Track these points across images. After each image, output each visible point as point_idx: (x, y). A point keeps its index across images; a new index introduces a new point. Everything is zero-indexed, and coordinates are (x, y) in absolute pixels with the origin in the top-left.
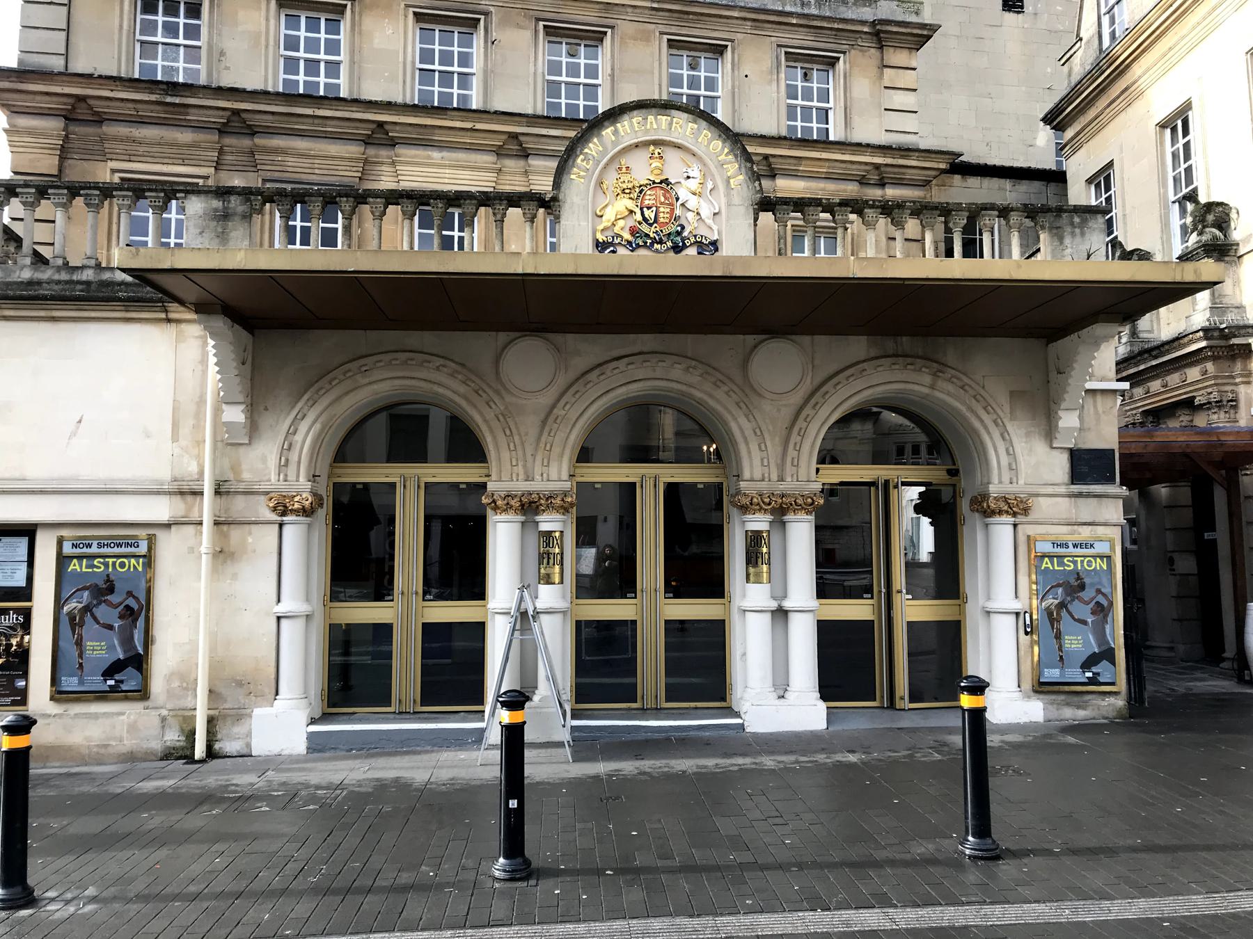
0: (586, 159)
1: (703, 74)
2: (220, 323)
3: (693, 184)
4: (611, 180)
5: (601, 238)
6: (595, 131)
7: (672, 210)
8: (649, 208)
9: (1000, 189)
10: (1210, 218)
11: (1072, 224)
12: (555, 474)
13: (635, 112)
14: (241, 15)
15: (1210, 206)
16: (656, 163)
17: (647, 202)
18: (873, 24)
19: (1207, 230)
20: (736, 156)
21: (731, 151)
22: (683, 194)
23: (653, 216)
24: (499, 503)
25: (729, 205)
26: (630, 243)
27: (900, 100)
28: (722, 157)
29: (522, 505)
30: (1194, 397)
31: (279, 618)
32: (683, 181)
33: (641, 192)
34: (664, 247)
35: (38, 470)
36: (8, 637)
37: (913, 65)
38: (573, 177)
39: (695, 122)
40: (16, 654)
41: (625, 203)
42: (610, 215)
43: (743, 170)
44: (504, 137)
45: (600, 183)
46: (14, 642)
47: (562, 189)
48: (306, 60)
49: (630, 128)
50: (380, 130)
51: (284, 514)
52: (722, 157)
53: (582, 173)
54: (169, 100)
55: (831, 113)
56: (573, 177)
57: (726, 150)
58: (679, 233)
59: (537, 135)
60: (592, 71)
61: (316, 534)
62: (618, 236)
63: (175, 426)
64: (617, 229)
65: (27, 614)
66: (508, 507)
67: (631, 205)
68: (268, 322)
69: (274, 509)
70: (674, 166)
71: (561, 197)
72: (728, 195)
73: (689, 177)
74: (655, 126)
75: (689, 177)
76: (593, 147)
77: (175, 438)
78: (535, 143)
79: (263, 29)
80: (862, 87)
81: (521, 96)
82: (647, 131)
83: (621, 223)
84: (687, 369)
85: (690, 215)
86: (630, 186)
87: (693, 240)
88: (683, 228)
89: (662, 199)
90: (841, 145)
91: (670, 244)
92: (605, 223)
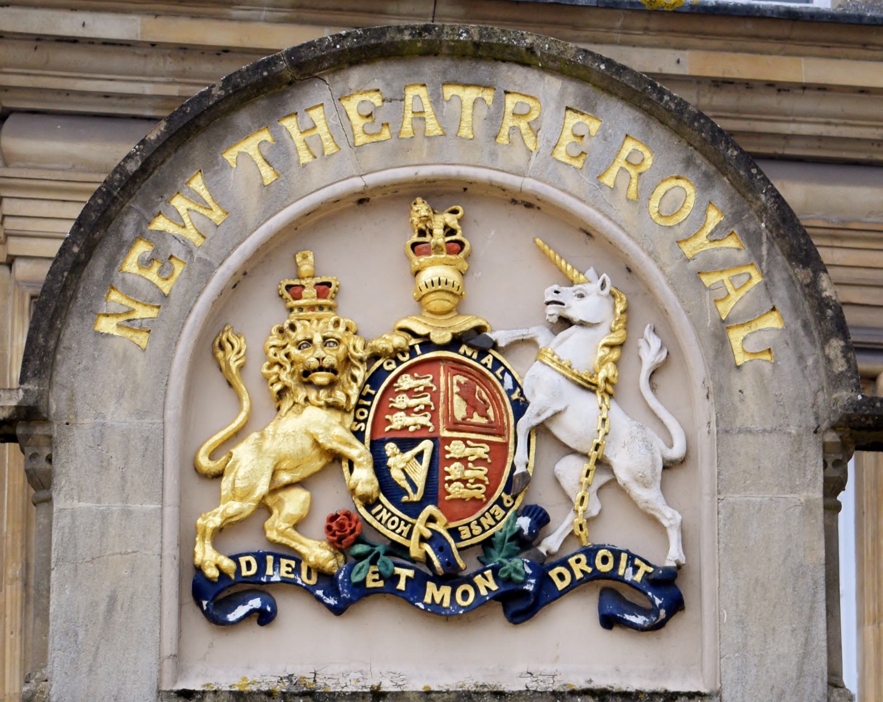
0: (160, 258)
3: (580, 350)
4: (256, 337)
5: (210, 558)
6: (197, 149)
7: (499, 452)
8: (406, 443)
13: (355, 76)
16: (436, 270)
17: (398, 420)
20: (751, 240)
22: (542, 385)
23: (420, 474)
25: (725, 429)
26: (326, 578)
28: (700, 244)
32: (542, 336)
33: (374, 380)
38: (106, 325)
39: (586, 108)
41: (311, 424)
42: (247, 469)
43: (781, 293)
44: (251, 226)
45: (211, 345)
47: (62, 373)
52: (700, 244)
53: (142, 313)
56: (106, 325)
57: (714, 217)
58: (523, 543)
59: (39, 39)
62: (282, 552)
64: (277, 528)
67: (334, 430)
70: (506, 283)
71: (56, 404)
72: (719, 391)
73: (565, 322)
74: (433, 127)
75: (565, 322)
76: (188, 211)
78: (26, 69)
82: (400, 149)
83: (295, 502)
84: (406, 428)
85: (571, 471)
86: (331, 357)
87: (580, 568)
88: (541, 519)
89: (460, 409)
91: (487, 584)
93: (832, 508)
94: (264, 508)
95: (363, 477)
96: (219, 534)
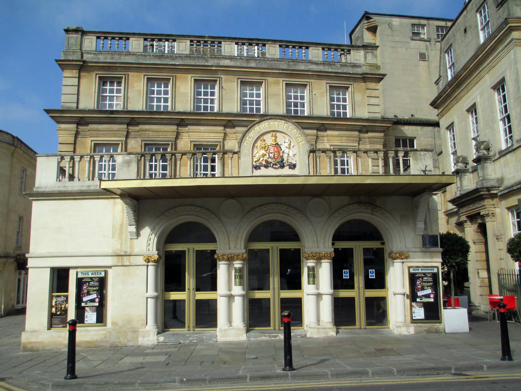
1: (299, 94)
2: (128, 200)
7: (279, 154)
8: (271, 153)
9: (416, 130)
10: (482, 147)
11: (420, 155)
12: (239, 248)
14: (135, 84)
15: (483, 142)
18: (362, 74)
19: (481, 151)
21: (300, 133)
24: (220, 257)
25: (299, 152)
27: (373, 101)
29: (228, 258)
30: (480, 212)
31: (147, 298)
32: (283, 144)
34: (277, 167)
35: (70, 250)
36: (61, 305)
37: (378, 88)
40: (64, 311)
41: (263, 152)
44: (226, 121)
46: (63, 306)
48: (157, 98)
49: (265, 126)
50: (182, 121)
51: (148, 262)
54: (110, 117)
55: (347, 106)
60: (258, 95)
61: (159, 270)
63: (113, 233)
65: (67, 297)
66: (223, 259)
68: (142, 204)
69: (145, 261)
72: (299, 148)
77: (113, 237)
79: (142, 89)
80: (358, 97)
81: (232, 106)
90: (350, 119)
91: (279, 166)
92: (255, 159)
93: (309, 158)
94: (259, 159)
95: (268, 156)
96: (255, 162)
